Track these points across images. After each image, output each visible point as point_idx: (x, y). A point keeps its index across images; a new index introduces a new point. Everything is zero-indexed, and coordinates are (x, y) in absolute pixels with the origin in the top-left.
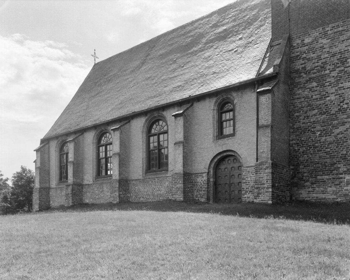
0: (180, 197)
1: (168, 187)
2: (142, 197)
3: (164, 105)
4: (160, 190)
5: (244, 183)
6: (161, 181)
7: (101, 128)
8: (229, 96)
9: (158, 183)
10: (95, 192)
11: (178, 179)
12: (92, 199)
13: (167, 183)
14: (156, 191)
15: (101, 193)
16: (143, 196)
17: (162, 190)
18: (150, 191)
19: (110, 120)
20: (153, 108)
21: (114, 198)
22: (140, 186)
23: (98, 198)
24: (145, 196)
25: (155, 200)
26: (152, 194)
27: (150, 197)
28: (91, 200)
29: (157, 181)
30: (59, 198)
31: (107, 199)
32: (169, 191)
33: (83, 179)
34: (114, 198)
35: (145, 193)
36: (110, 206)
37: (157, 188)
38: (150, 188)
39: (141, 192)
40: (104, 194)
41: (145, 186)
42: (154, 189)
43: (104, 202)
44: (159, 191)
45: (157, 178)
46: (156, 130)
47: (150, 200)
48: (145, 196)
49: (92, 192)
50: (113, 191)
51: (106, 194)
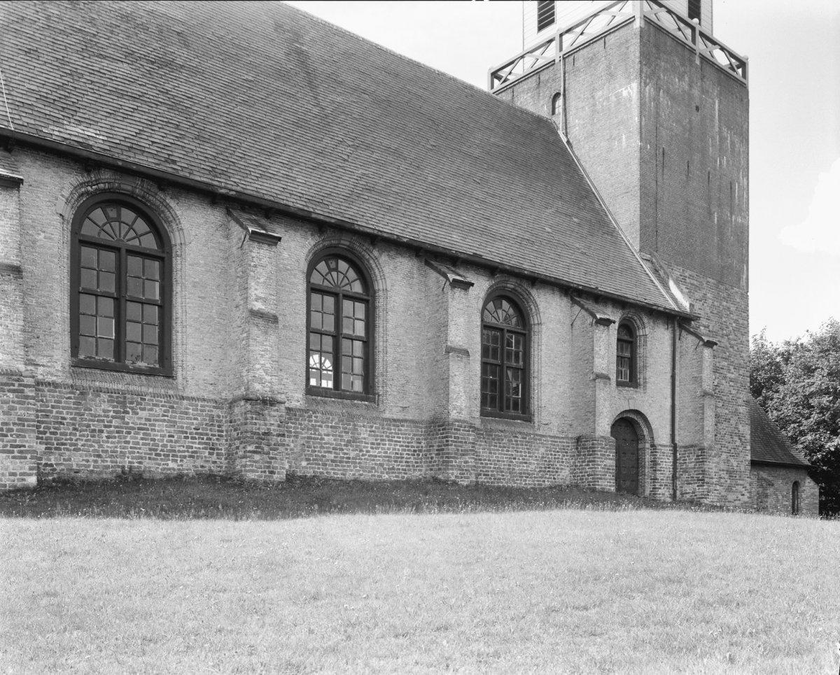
0: (610, 486)
1: (543, 457)
2: (484, 475)
3: (548, 278)
4: (526, 463)
5: (660, 471)
6: (529, 442)
7: (341, 239)
8: (636, 318)
9: (522, 445)
10: (322, 439)
11: (608, 449)
12: (308, 460)
13: (542, 450)
14: (517, 462)
15: (346, 445)
16: (486, 471)
17: (530, 463)
18: (504, 461)
19: (405, 240)
20: (526, 272)
21: (463, 470)
22: (480, 445)
23: (332, 461)
24: (492, 471)
25: (515, 483)
26: (509, 469)
27: (503, 476)
28: (304, 463)
29: (520, 441)
30: (105, 435)
31: (373, 468)
32: (545, 468)
33: (594, 430)
34: (463, 470)
35: (491, 464)
36: (558, 495)
37: (521, 458)
38: (504, 454)
39: (480, 460)
40: (361, 451)
41: (493, 447)
42: (515, 459)
43: (361, 475)
44: (525, 465)
45: (520, 433)
46: (328, 280)
47: (502, 483)
48: (492, 471)
49: (308, 438)
50: (458, 450)
51: (368, 451)
